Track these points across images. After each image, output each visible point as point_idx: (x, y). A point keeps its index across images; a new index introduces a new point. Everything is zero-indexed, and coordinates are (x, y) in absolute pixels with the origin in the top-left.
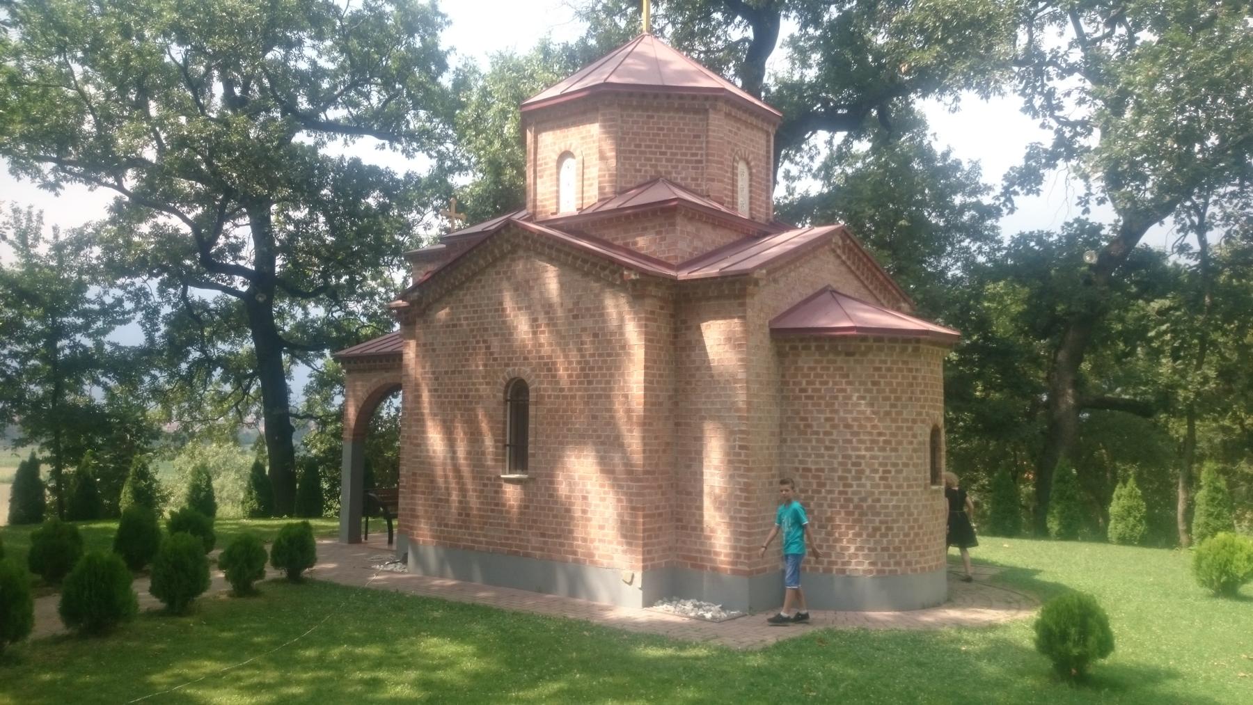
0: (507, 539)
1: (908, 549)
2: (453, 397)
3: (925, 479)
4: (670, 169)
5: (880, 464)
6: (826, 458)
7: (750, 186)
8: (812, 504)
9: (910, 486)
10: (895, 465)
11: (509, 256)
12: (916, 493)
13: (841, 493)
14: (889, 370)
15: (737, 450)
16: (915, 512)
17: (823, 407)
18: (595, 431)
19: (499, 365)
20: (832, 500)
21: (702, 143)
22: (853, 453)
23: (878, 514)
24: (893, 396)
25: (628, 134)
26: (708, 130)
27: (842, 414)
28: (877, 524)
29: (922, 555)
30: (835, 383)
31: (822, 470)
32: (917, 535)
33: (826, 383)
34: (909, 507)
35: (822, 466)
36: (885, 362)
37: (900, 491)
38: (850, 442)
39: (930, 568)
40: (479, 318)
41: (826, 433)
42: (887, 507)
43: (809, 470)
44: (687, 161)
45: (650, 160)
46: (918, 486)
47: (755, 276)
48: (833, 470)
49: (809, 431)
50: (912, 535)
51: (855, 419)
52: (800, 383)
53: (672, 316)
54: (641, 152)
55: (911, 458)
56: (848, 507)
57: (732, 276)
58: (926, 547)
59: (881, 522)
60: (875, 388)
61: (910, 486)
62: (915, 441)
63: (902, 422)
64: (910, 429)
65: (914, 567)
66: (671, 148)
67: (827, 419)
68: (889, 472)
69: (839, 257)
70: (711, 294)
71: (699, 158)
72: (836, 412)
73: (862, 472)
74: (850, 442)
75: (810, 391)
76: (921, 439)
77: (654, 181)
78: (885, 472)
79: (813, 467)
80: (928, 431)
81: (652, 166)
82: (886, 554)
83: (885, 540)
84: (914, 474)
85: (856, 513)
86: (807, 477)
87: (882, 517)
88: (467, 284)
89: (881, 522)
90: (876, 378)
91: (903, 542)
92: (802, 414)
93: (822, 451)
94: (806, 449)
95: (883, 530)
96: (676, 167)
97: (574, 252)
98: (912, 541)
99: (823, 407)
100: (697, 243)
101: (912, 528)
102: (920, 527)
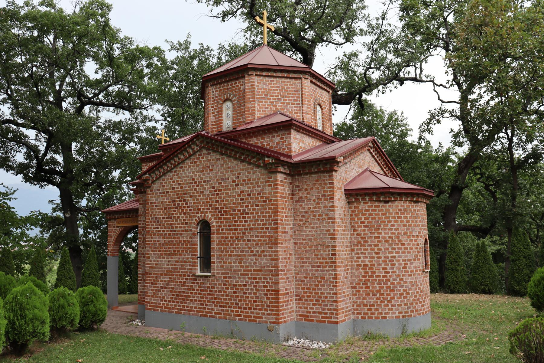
0: (200, 308)
1: (416, 303)
2: (167, 231)
4: (283, 107)
5: (403, 261)
7: (322, 118)
9: (416, 271)
10: (410, 260)
11: (198, 153)
12: (419, 274)
13: (384, 276)
14: (405, 210)
15: (330, 256)
16: (419, 284)
17: (373, 231)
18: (249, 248)
19: (193, 213)
20: (379, 280)
21: (299, 94)
23: (402, 287)
24: (407, 224)
25: (261, 89)
26: (302, 88)
27: (383, 234)
28: (402, 292)
29: (422, 306)
31: (374, 265)
32: (420, 296)
34: (416, 281)
35: (374, 263)
36: (403, 206)
37: (412, 273)
38: (388, 249)
39: (426, 312)
40: (181, 188)
41: (375, 245)
42: (406, 282)
43: (367, 265)
44: (292, 104)
45: (273, 102)
46: (420, 270)
47: (338, 160)
48: (380, 265)
49: (366, 244)
51: (390, 237)
52: (361, 219)
53: (291, 183)
54: (268, 99)
57: (325, 160)
59: (404, 290)
60: (399, 220)
61: (416, 271)
64: (416, 241)
66: (284, 97)
67: (376, 238)
68: (407, 264)
69: (371, 153)
70: (313, 171)
71: (298, 102)
72: (380, 233)
73: (394, 265)
74: (388, 249)
75: (366, 222)
76: (420, 246)
77: (275, 114)
78: (405, 264)
79: (369, 264)
81: (273, 106)
82: (406, 307)
83: (406, 300)
87: (404, 288)
88: (175, 170)
89: (404, 290)
91: (414, 300)
92: (362, 236)
93: (374, 255)
94: (365, 254)
95: (405, 295)
96: (286, 107)
97: (236, 150)
98: (418, 299)
100: (302, 145)
101: (418, 292)
102: (421, 292)
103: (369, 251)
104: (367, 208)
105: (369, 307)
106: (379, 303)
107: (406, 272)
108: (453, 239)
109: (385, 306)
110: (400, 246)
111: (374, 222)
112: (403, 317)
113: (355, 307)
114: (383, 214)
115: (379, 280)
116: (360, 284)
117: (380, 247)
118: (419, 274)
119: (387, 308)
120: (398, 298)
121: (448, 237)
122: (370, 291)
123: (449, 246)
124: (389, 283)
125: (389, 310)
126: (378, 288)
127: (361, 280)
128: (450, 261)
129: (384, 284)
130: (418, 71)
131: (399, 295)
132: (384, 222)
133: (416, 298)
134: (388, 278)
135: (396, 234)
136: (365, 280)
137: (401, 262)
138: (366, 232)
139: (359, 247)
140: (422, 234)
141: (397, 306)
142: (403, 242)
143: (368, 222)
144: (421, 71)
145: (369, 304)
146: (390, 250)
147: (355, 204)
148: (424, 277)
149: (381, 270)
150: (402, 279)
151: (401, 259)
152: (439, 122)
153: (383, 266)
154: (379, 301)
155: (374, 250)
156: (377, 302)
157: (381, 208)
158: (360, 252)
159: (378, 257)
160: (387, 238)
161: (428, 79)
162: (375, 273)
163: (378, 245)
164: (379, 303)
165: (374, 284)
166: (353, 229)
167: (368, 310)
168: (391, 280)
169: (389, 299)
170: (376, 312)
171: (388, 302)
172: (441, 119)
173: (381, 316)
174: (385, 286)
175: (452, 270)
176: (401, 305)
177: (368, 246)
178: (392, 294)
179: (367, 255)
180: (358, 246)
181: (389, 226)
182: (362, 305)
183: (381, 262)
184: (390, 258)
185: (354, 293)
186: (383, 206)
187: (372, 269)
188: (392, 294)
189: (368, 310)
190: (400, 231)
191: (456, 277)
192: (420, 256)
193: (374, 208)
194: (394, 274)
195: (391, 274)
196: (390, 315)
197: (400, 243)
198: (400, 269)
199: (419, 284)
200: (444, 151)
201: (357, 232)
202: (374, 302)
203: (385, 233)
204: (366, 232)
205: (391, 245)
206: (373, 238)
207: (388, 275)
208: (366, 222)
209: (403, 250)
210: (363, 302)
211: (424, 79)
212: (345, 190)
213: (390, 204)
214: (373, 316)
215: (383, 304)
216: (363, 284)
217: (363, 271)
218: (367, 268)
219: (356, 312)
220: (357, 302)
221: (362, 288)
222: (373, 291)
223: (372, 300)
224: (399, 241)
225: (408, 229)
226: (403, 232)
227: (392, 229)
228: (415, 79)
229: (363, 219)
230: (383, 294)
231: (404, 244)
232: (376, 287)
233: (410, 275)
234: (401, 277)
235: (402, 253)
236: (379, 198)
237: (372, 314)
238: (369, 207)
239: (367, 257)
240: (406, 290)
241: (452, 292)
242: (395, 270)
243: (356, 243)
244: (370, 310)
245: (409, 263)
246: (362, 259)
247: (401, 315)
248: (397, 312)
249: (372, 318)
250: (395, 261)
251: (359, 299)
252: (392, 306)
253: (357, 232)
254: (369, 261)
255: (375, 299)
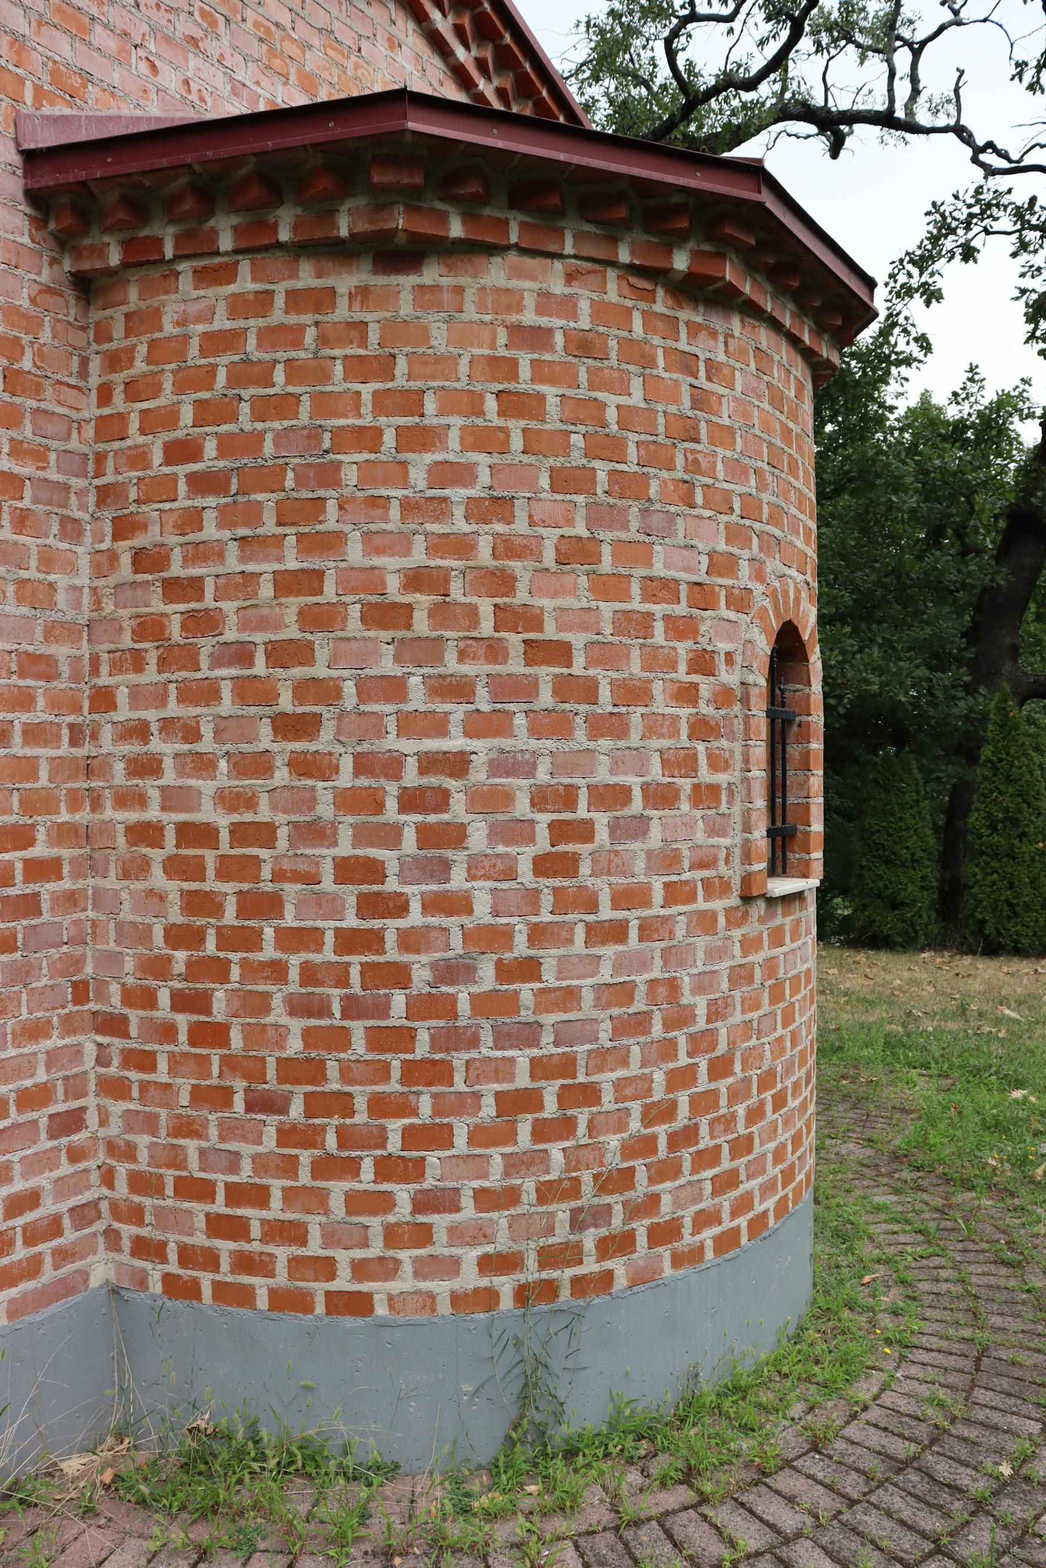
1: (666, 1171)
3: (747, 857)
5: (540, 800)
6: (282, 776)
8: (220, 997)
9: (675, 893)
12: (706, 922)
13: (348, 941)
17: (269, 526)
20: (310, 974)
22: (408, 746)
23: (529, 1035)
24: (602, 470)
27: (355, 553)
28: (522, 1080)
29: (726, 1182)
30: (324, 405)
31: (265, 834)
32: (703, 1103)
33: (285, 405)
34: (673, 986)
35: (264, 813)
36: (567, 307)
37: (633, 917)
38: (395, 689)
42: (570, 997)
43: (205, 835)
46: (715, 888)
49: (206, 646)
50: (683, 1110)
51: (416, 580)
52: (169, 418)
55: (687, 764)
56: (382, 1009)
58: (742, 1146)
59: (540, 1068)
60: (515, 426)
61: (675, 893)
62: (706, 687)
63: (649, 596)
65: (688, 1239)
68: (584, 832)
72: (334, 542)
73: (456, 836)
74: (395, 689)
75: (210, 448)
76: (729, 677)
78: (559, 831)
79: (223, 821)
80: (764, 646)
82: (562, 1212)
83: (556, 1151)
84: (700, 836)
85: (423, 1038)
86: (196, 871)
87: (547, 1047)
89: (540, 1068)
90: (524, 380)
92: (177, 569)
93: (265, 739)
94: (192, 734)
95: (551, 1108)
99: (269, 526)
103: (227, 705)
104: (221, 322)
105: (220, 1206)
106: (305, 1178)
107: (563, 902)
108: (1006, 725)
109: (356, 1203)
110: (516, 666)
111: (280, 437)
112: (522, 1295)
113: (122, 1188)
114: (360, 370)
115: (310, 974)
116: (148, 1000)
117: (320, 670)
118: (706, 922)
119: (375, 1223)
120: (479, 1136)
121: (984, 718)
122: (228, 1062)
123: (986, 752)
124: (399, 1000)
125: (392, 1236)
126: (294, 1046)
127: (159, 967)
128: (989, 816)
129: (352, 1008)
130: (903, 89)
131: (488, 1109)
132: (370, 438)
133: (662, 1130)
134: (392, 954)
135: (484, 555)
136: (196, 969)
137: (522, 807)
138: (211, 531)
139: (151, 675)
140: (744, 575)
141: (468, 1210)
142: (550, 631)
143: (226, 446)
144: (916, 92)
145: (221, 1179)
146: (417, 699)
147: (133, 294)
148: (750, 945)
149: (328, 883)
150: (529, 969)
151: (521, 788)
152: (969, 253)
153: (345, 848)
154: (305, 1157)
155: (269, 697)
156: (290, 1167)
157: (342, 311)
158: (151, 715)
159: (301, 765)
160: (393, 584)
161: (942, 121)
162: (272, 905)
163: (302, 653)
164: (305, 1178)
165: (262, 1004)
166: (108, 514)
167: (218, 1226)
168: (421, 976)
169: (394, 1144)
170: (282, 1253)
171: (386, 1169)
172: (976, 243)
173: (320, 1288)
174: (358, 1029)
175: (996, 856)
176: (511, 1197)
177: (217, 662)
178: (425, 1105)
179: (207, 745)
180: (138, 664)
181: (418, 476)
182: (169, 1176)
183: (325, 810)
184: (411, 777)
185: (113, 1070)
186: (362, 294)
187: (246, 869)
188: (425, 1105)
189: (218, 1226)
190: (521, 526)
191: (1011, 886)
192: (717, 763)
193: (278, 315)
194: (452, 922)
195: (415, 917)
196: (404, 1283)
197: (514, 640)
198: (510, 874)
199: (701, 1005)
200: (989, 396)
201: (140, 541)
202: (261, 1163)
203: (373, 543)
204: (211, 531)
205: (432, 650)
206: (266, 590)
207: (392, 925)
208: (210, 448)
209: (546, 698)
210: (177, 1160)
211: (923, 118)
212: (32, 158)
213: (432, 274)
214: (261, 1285)
215: (338, 1189)
216: (181, 1002)
217: (174, 888)
218: (210, 857)
219: (128, 1231)
220: (129, 1153)
221: (168, 1032)
222: (254, 1072)
223: (247, 1150)
224: (506, 618)
225: (597, 517)
226: (551, 536)
227: (440, 508)
228: (885, 119)
229: (187, 415)
230: (343, 1103)
231: (562, 653)
232: (282, 1034)
233: (617, 932)
234: (521, 947)
235: (536, 732)
236: (329, 216)
237: (245, 1263)
238: (238, 306)
239: (204, 765)
240: (567, 1066)
241: (992, 950)
242: (458, 881)
243: (127, 641)
244: (236, 1229)
245: (602, 820)
246: (169, 777)
247: (505, 1285)
248: (470, 1256)
249: (244, 1296)
250: (458, 803)
251: (150, 1124)
252: (423, 1203)
253: (140, 541)
254: (229, 800)
255: (270, 1136)
